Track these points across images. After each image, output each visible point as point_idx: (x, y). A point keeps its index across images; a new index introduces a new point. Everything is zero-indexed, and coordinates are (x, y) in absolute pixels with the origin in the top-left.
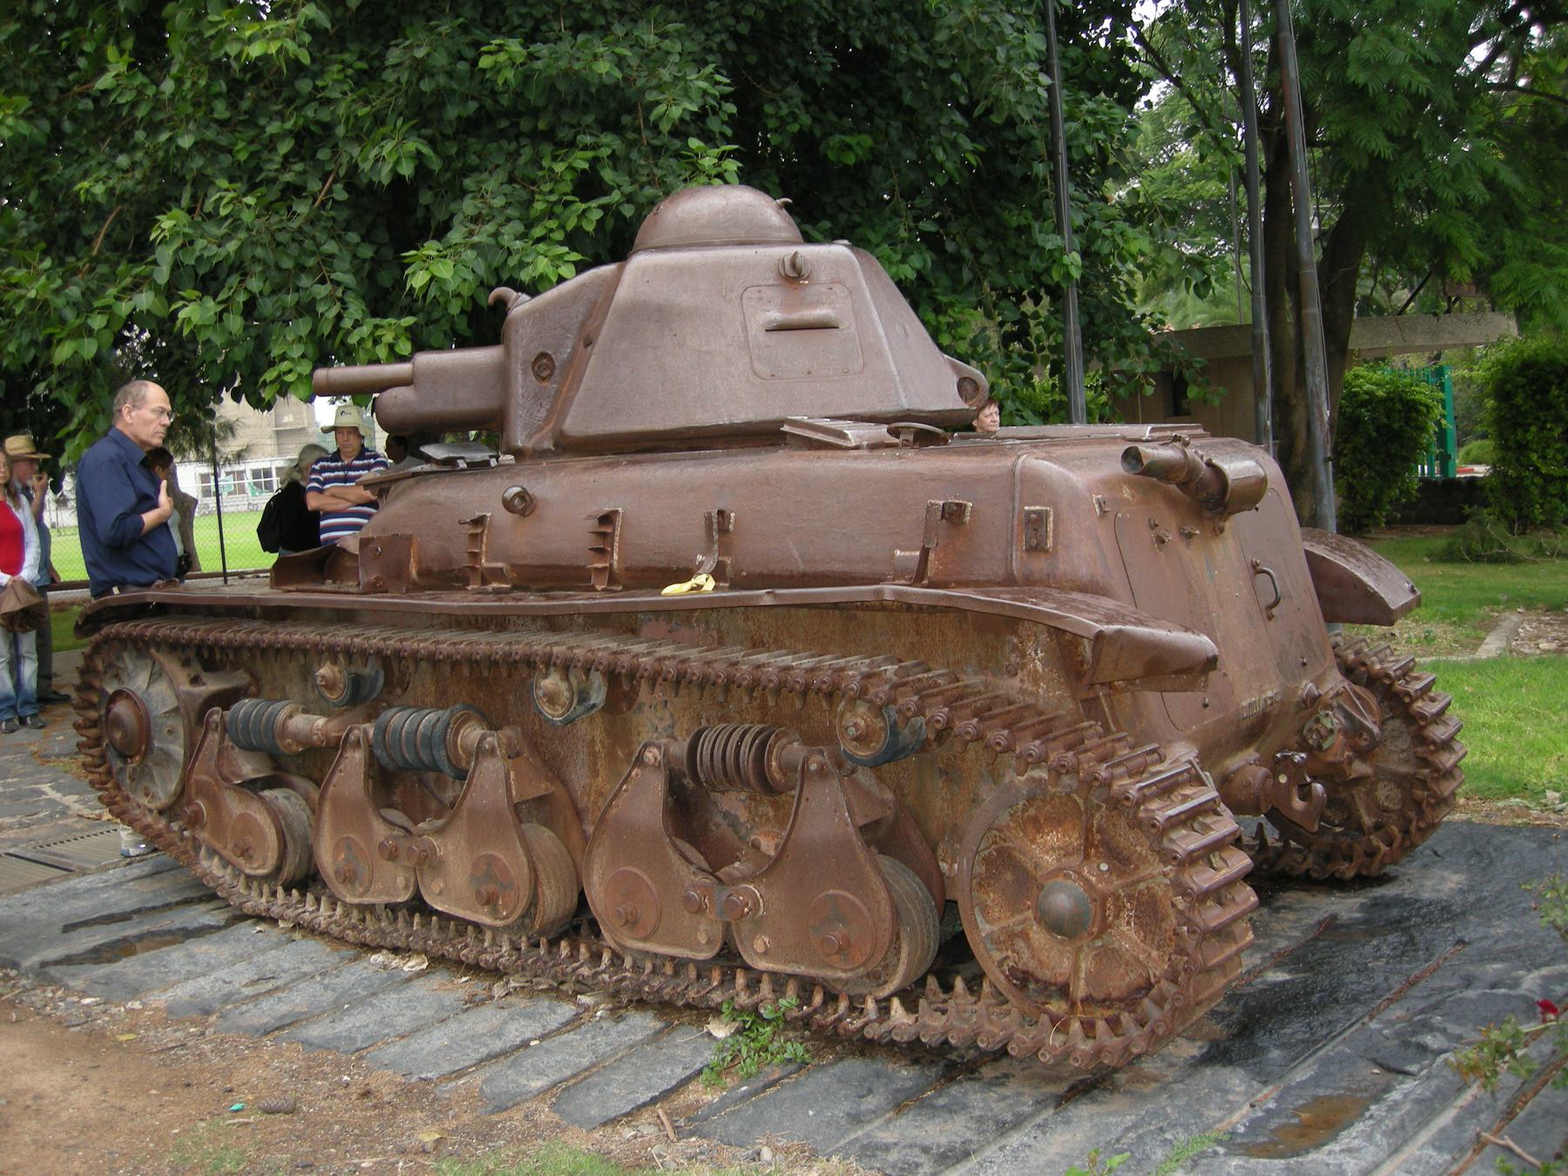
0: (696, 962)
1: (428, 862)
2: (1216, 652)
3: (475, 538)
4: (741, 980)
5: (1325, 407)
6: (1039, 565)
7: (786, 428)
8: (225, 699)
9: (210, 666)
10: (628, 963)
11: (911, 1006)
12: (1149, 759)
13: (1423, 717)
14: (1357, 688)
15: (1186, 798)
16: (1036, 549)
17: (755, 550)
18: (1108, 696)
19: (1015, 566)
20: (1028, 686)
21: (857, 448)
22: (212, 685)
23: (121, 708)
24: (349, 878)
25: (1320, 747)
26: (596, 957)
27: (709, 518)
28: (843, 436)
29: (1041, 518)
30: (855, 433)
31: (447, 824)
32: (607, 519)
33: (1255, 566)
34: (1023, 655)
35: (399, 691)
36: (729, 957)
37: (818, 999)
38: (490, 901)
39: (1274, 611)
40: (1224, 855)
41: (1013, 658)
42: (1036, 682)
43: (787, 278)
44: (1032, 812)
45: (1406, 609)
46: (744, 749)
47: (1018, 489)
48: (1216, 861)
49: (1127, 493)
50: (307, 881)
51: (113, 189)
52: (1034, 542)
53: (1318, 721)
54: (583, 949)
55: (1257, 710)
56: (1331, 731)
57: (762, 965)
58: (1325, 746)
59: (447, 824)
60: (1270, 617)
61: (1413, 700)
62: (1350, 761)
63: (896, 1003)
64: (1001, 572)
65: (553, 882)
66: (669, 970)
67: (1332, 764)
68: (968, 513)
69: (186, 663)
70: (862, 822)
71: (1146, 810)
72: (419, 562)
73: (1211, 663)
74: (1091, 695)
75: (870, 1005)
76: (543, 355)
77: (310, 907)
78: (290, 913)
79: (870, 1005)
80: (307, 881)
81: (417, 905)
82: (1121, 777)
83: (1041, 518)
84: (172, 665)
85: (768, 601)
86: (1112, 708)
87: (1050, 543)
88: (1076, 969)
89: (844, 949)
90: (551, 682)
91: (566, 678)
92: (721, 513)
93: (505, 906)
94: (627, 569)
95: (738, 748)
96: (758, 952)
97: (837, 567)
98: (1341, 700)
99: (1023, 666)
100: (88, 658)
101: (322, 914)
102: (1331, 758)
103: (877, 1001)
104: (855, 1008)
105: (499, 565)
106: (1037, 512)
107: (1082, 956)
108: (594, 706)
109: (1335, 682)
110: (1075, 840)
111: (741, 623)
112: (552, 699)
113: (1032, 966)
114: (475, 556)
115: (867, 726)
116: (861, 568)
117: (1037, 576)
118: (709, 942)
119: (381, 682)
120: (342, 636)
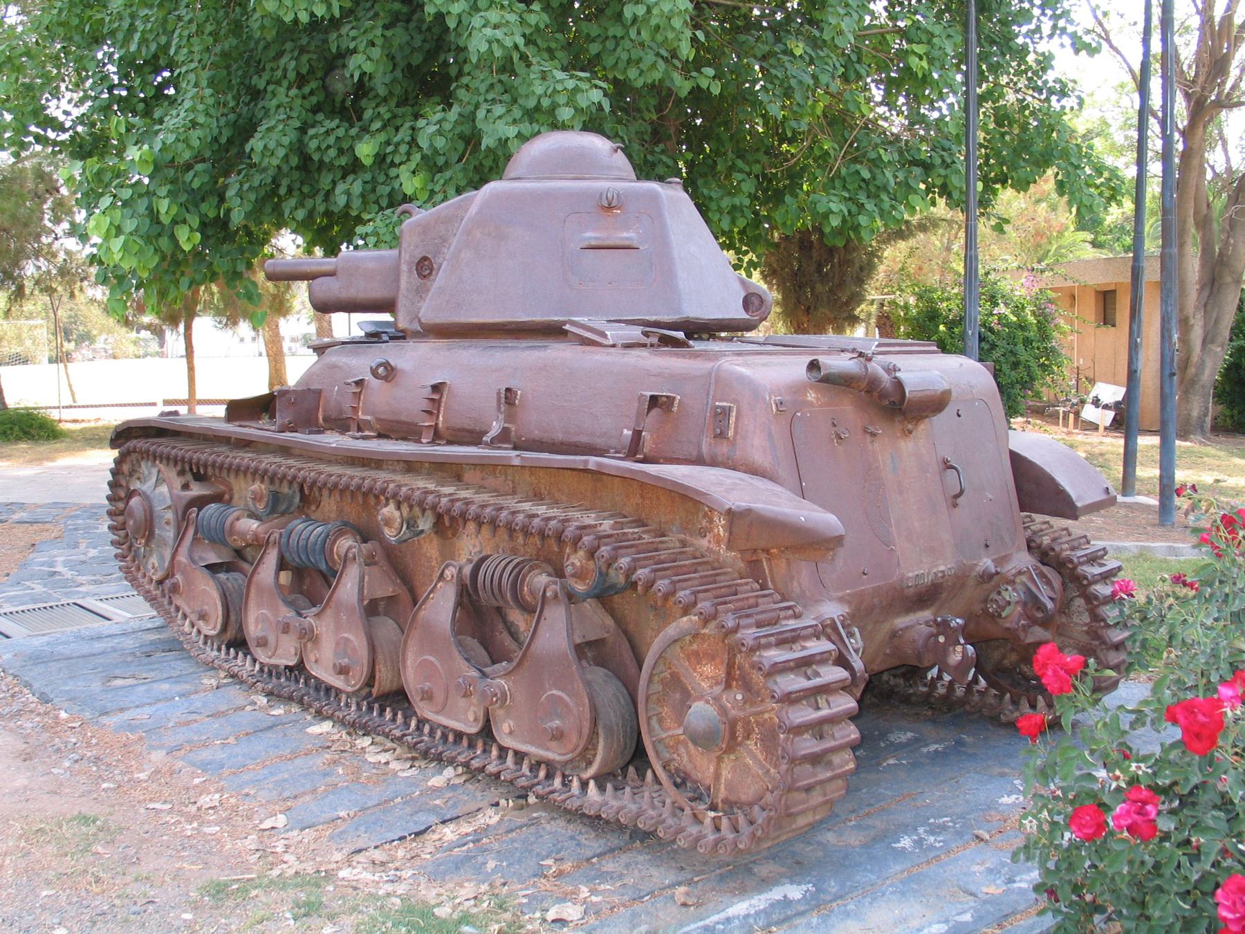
0: (469, 735)
1: (308, 636)
2: (842, 531)
3: (357, 395)
4: (495, 752)
5: (1174, 331)
6: (723, 449)
7: (567, 327)
8: (200, 502)
9: (199, 477)
10: (427, 729)
11: (601, 788)
12: (782, 614)
13: (1096, 598)
14: (1045, 569)
15: (804, 648)
16: (721, 436)
17: (532, 423)
18: (769, 560)
19: (705, 449)
20: (713, 546)
21: (614, 346)
22: (197, 490)
23: (135, 501)
24: (262, 643)
25: (1000, 615)
26: (407, 720)
27: (499, 394)
28: (603, 335)
29: (726, 412)
30: (614, 333)
31: (323, 610)
32: (437, 388)
33: (945, 462)
34: (711, 521)
35: (313, 508)
36: (487, 732)
37: (542, 774)
38: (343, 671)
39: (959, 500)
40: (831, 699)
41: (704, 523)
42: (718, 543)
43: (603, 207)
44: (695, 647)
45: (1094, 507)
46: (506, 575)
47: (712, 388)
48: (821, 701)
49: (811, 396)
50: (239, 643)
51: (444, 110)
52: (718, 431)
53: (999, 593)
54: (399, 716)
55: (928, 580)
56: (1009, 603)
57: (507, 742)
58: (1004, 614)
59: (323, 610)
60: (955, 506)
61: (1090, 584)
62: (1025, 629)
63: (592, 784)
64: (695, 453)
65: (389, 664)
66: (451, 738)
67: (1008, 629)
68: (677, 402)
69: (181, 473)
70: (578, 641)
71: (760, 656)
72: (324, 411)
73: (839, 540)
74: (754, 558)
75: (575, 784)
76: (425, 259)
77: (239, 662)
78: (226, 666)
79: (575, 784)
80: (239, 643)
81: (298, 669)
82: (748, 626)
83: (726, 412)
84: (171, 473)
85: (516, 462)
86: (771, 570)
87: (731, 433)
88: (717, 776)
89: (558, 736)
90: (389, 511)
91: (399, 508)
92: (508, 390)
93: (354, 678)
94: (448, 429)
95: (501, 576)
96: (504, 732)
97: (584, 439)
98: (1024, 578)
99: (711, 530)
100: (118, 462)
101: (243, 666)
102: (1008, 625)
103: (580, 779)
104: (566, 784)
105: (369, 418)
106: (723, 408)
107: (723, 765)
108: (422, 531)
109: (1023, 560)
110: (722, 673)
111: (527, 476)
112: (388, 522)
113: (689, 767)
114: (355, 409)
115: (582, 566)
116: (599, 442)
117: (720, 459)
118: (476, 720)
119: (297, 499)
120: (268, 462)
